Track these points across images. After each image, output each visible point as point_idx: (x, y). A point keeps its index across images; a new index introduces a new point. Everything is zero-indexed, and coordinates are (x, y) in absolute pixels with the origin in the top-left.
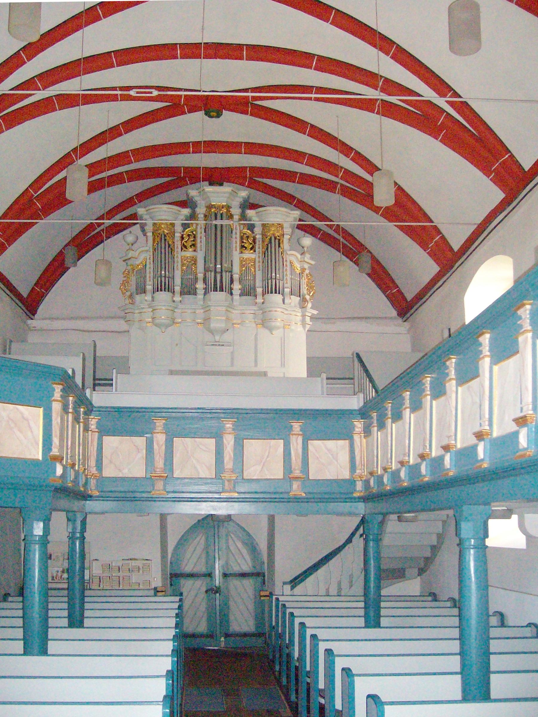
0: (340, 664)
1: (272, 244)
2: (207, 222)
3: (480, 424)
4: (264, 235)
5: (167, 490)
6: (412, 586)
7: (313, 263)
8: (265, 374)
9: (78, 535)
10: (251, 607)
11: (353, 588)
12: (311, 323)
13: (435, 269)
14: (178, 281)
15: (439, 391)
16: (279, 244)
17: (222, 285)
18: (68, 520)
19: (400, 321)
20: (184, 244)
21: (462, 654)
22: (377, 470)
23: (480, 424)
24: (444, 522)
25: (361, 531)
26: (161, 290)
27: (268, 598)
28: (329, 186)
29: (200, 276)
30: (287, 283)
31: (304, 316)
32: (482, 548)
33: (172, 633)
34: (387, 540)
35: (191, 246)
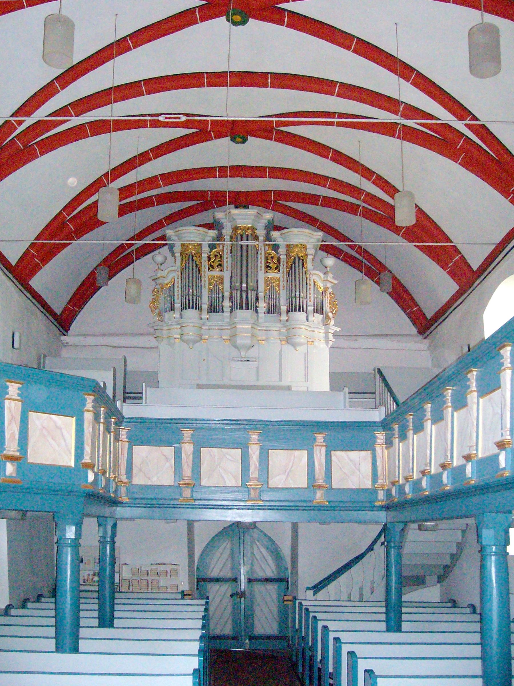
0: (362, 665)
1: (296, 264)
2: (233, 243)
3: (502, 434)
4: (288, 255)
5: (194, 498)
6: (432, 593)
8: (289, 388)
9: (109, 540)
10: (275, 610)
11: (374, 594)
12: (334, 340)
13: (453, 287)
14: (205, 299)
15: (460, 403)
16: (303, 264)
17: (248, 304)
18: (99, 525)
19: (420, 337)
21: (483, 658)
22: (399, 480)
23: (502, 434)
24: (464, 532)
25: (382, 539)
26: (189, 308)
27: (291, 602)
28: (352, 209)
29: (227, 294)
30: (310, 301)
31: (327, 333)
32: (503, 555)
33: (199, 634)
34: (406, 550)
35: (217, 266)
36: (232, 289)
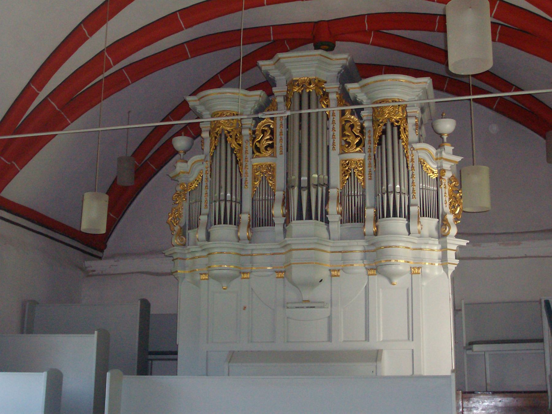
1: (384, 134)
4: (374, 121)
7: (458, 159)
12: (457, 262)
16: (399, 133)
20: (256, 145)
29: (279, 195)
30: (414, 197)
31: (444, 250)
35: (266, 148)
36: (288, 187)
